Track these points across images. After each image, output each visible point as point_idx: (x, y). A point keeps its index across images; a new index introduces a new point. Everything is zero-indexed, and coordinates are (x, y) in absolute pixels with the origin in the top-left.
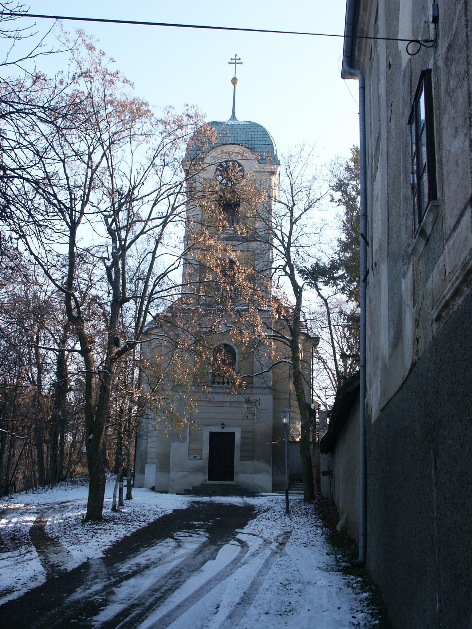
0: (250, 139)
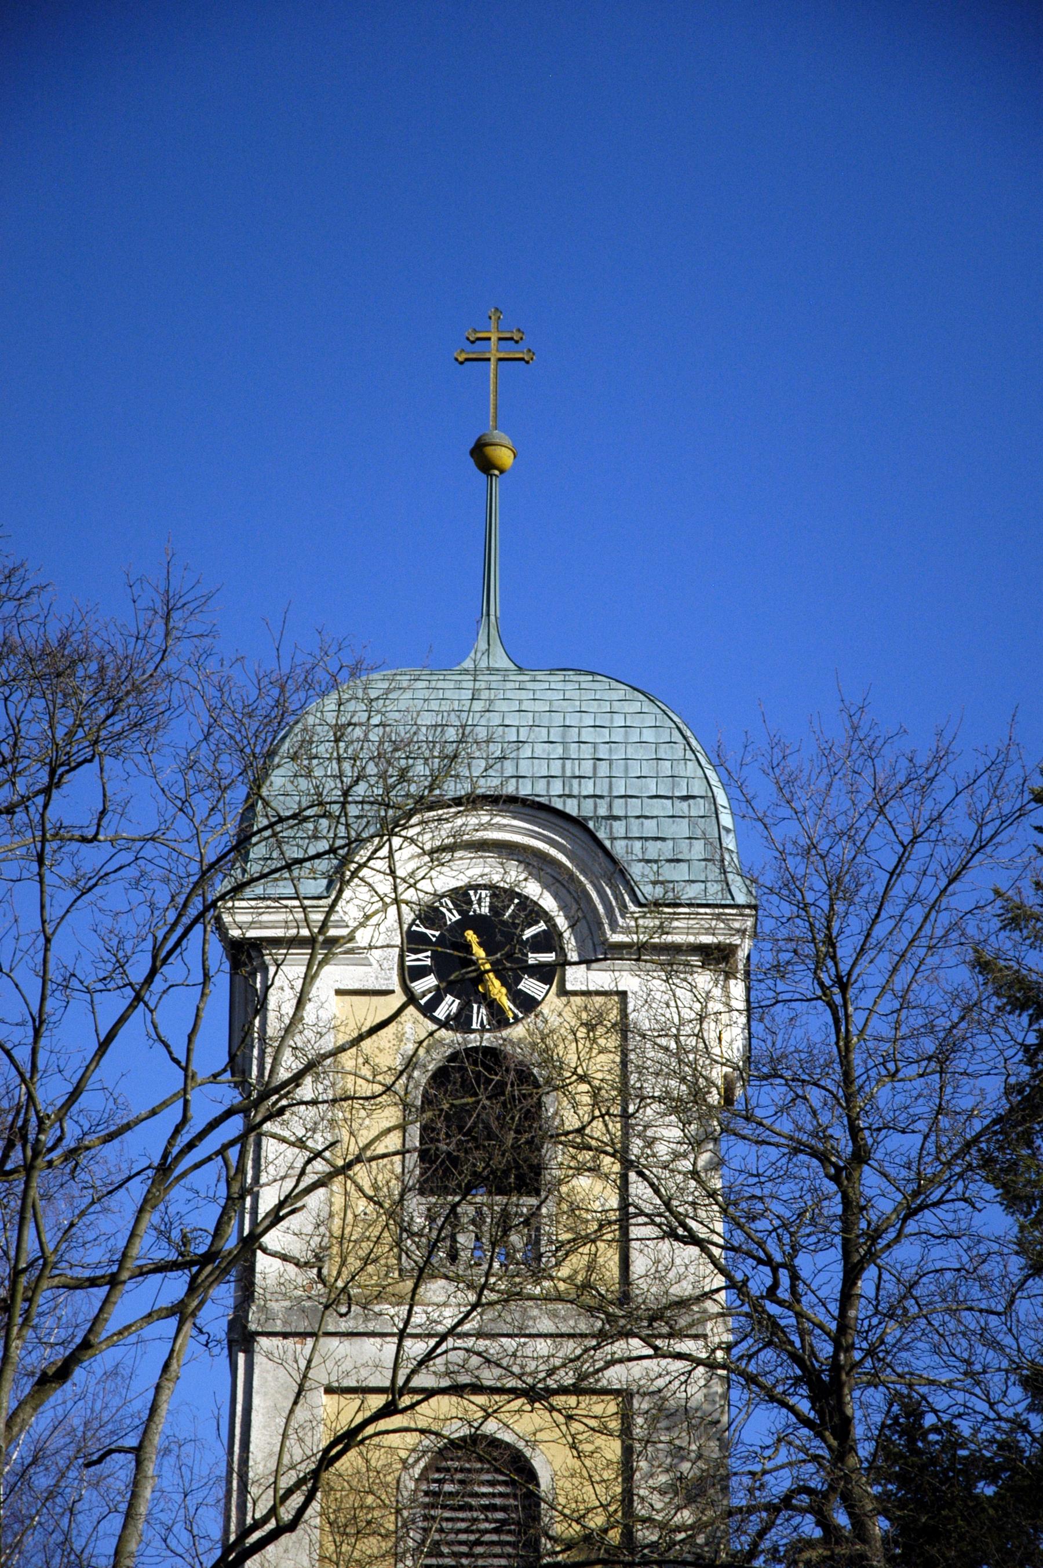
0: (587, 768)
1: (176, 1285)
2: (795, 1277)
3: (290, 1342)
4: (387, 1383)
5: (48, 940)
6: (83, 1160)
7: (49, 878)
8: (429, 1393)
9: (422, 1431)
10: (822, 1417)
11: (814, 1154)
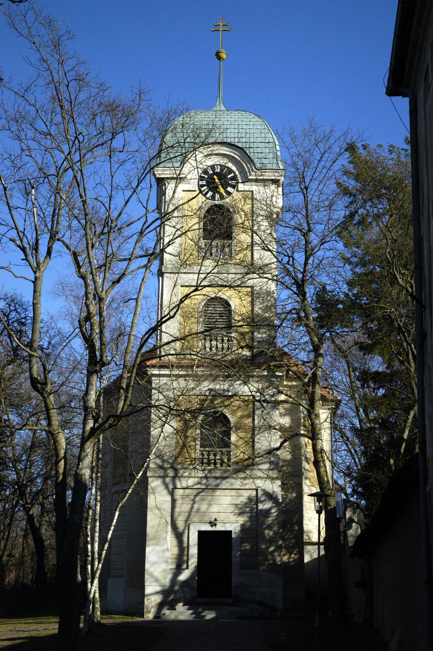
0: (244, 135)
1: (144, 261)
2: (293, 259)
3: (172, 275)
4: (195, 284)
5: (112, 177)
6: (122, 230)
7: (112, 161)
8: (205, 286)
9: (204, 295)
10: (299, 292)
11: (299, 230)
